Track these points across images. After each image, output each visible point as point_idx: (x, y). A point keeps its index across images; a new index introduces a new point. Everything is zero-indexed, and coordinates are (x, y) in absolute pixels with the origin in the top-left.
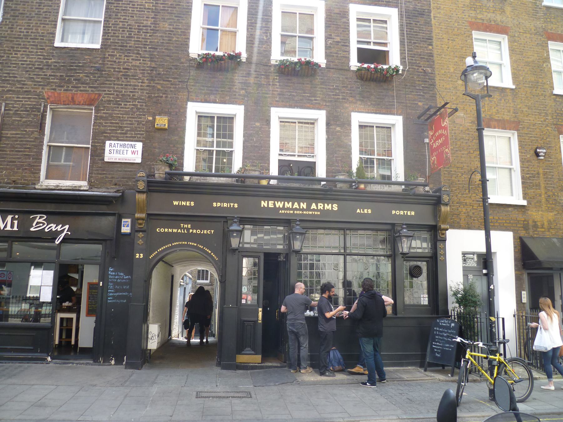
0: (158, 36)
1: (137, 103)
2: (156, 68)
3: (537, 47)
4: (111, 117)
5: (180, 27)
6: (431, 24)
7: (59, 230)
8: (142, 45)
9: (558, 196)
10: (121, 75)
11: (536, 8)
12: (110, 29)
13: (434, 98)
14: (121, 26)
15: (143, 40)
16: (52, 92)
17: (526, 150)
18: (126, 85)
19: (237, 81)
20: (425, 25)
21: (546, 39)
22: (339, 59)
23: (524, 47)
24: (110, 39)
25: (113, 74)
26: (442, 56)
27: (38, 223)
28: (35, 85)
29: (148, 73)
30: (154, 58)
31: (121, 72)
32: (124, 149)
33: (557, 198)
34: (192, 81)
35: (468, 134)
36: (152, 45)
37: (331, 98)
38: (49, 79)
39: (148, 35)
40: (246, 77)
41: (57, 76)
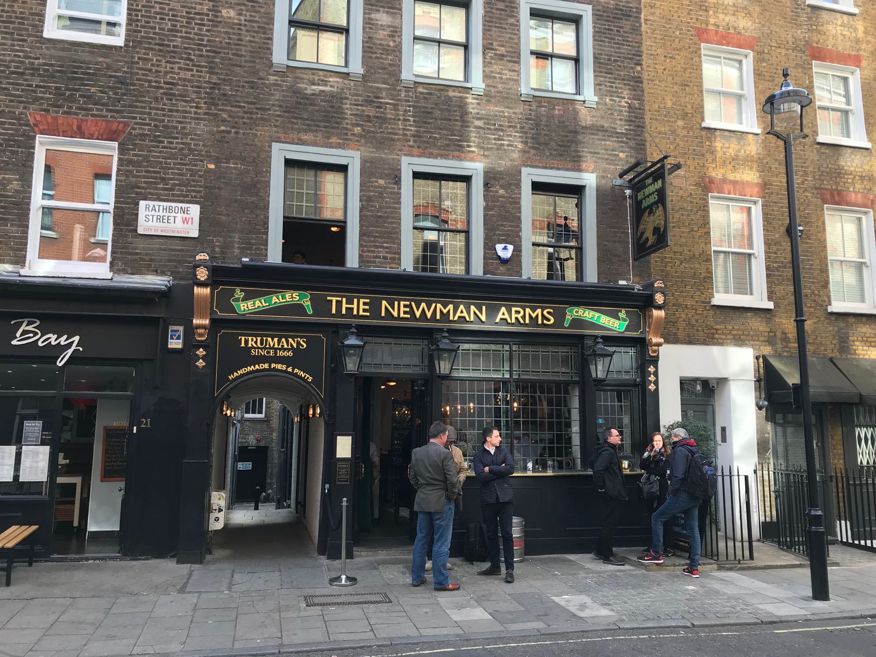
0: (220, 31)
1: (189, 141)
2: (218, 84)
3: (795, 70)
4: (147, 162)
5: (257, 19)
6: (641, 31)
7: (63, 343)
8: (195, 44)
9: (819, 296)
10: (161, 94)
11: (796, 8)
12: (140, 14)
13: (642, 147)
14: (158, 10)
15: (196, 37)
16: (41, 115)
17: (774, 228)
18: (170, 111)
19: (349, 112)
20: (631, 33)
21: (809, 58)
22: (503, 83)
23: (777, 69)
24: (140, 32)
25: (149, 91)
26: (655, 82)
27: (25, 332)
28: (11, 101)
29: (206, 93)
30: (214, 68)
31: (162, 88)
32: (170, 214)
33: (817, 298)
34: (278, 109)
35: (691, 202)
36: (211, 46)
37: (492, 144)
38: (35, 92)
39: (205, 28)
40: (362, 105)
41: (50, 87)
